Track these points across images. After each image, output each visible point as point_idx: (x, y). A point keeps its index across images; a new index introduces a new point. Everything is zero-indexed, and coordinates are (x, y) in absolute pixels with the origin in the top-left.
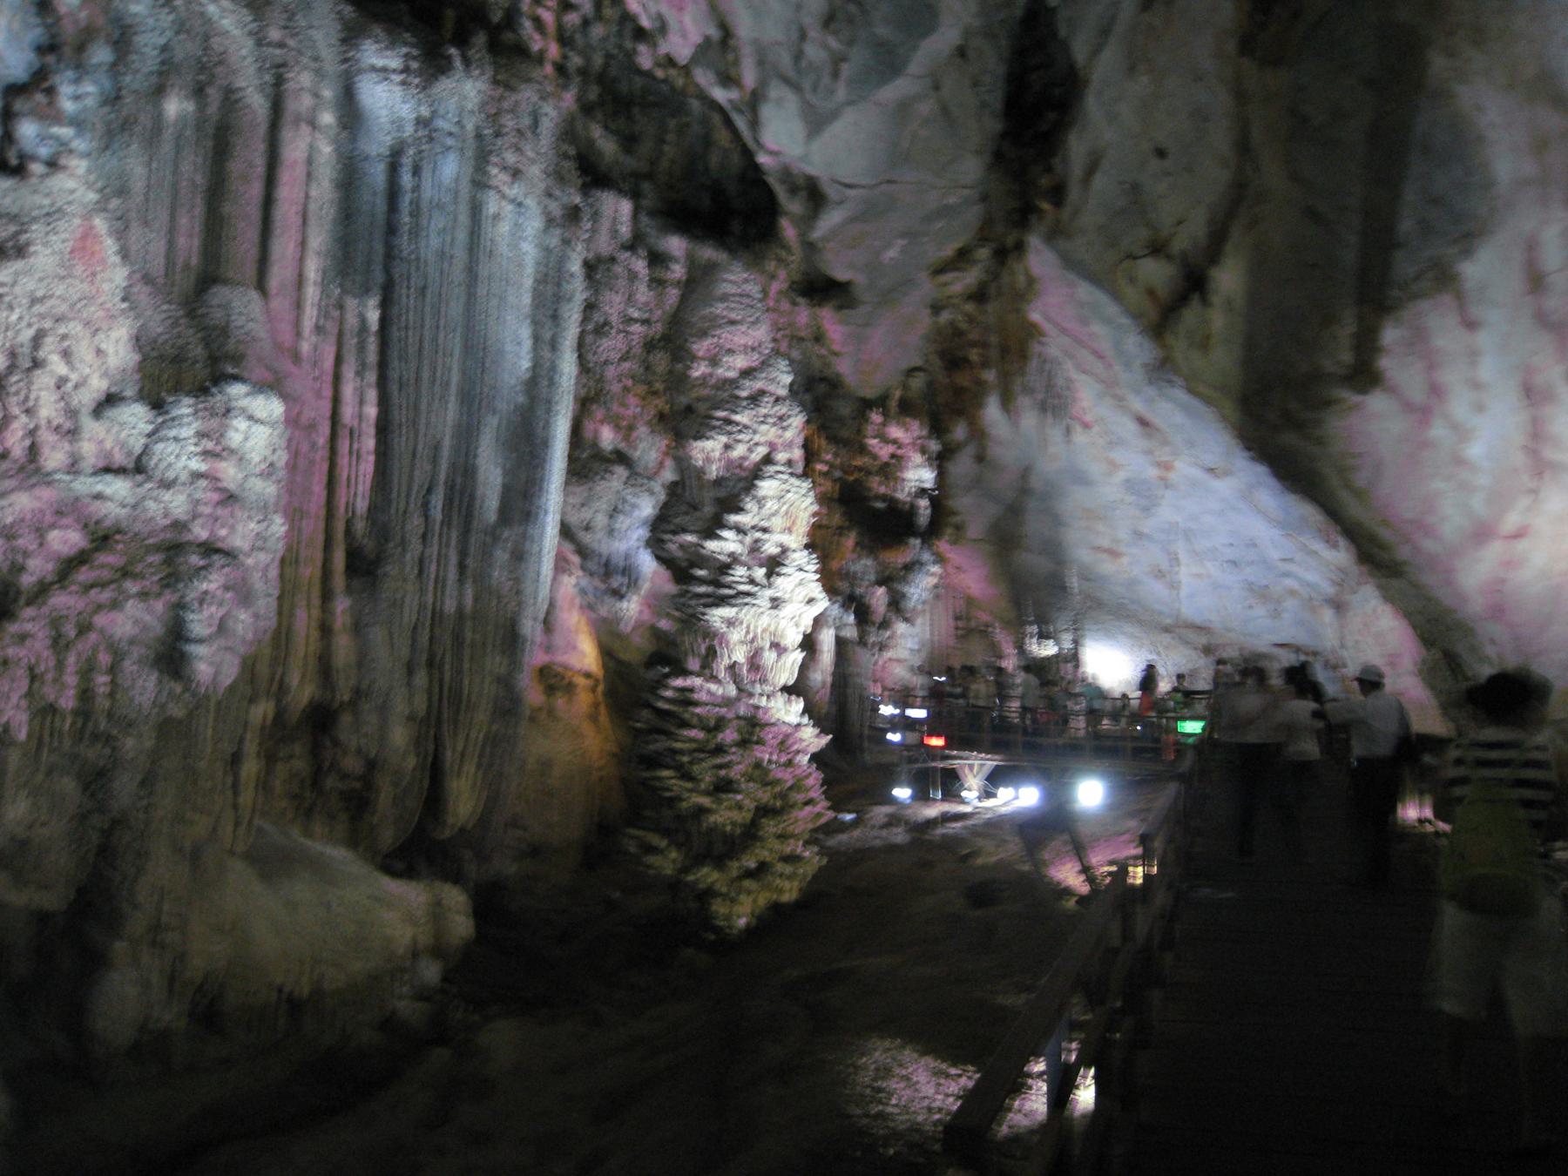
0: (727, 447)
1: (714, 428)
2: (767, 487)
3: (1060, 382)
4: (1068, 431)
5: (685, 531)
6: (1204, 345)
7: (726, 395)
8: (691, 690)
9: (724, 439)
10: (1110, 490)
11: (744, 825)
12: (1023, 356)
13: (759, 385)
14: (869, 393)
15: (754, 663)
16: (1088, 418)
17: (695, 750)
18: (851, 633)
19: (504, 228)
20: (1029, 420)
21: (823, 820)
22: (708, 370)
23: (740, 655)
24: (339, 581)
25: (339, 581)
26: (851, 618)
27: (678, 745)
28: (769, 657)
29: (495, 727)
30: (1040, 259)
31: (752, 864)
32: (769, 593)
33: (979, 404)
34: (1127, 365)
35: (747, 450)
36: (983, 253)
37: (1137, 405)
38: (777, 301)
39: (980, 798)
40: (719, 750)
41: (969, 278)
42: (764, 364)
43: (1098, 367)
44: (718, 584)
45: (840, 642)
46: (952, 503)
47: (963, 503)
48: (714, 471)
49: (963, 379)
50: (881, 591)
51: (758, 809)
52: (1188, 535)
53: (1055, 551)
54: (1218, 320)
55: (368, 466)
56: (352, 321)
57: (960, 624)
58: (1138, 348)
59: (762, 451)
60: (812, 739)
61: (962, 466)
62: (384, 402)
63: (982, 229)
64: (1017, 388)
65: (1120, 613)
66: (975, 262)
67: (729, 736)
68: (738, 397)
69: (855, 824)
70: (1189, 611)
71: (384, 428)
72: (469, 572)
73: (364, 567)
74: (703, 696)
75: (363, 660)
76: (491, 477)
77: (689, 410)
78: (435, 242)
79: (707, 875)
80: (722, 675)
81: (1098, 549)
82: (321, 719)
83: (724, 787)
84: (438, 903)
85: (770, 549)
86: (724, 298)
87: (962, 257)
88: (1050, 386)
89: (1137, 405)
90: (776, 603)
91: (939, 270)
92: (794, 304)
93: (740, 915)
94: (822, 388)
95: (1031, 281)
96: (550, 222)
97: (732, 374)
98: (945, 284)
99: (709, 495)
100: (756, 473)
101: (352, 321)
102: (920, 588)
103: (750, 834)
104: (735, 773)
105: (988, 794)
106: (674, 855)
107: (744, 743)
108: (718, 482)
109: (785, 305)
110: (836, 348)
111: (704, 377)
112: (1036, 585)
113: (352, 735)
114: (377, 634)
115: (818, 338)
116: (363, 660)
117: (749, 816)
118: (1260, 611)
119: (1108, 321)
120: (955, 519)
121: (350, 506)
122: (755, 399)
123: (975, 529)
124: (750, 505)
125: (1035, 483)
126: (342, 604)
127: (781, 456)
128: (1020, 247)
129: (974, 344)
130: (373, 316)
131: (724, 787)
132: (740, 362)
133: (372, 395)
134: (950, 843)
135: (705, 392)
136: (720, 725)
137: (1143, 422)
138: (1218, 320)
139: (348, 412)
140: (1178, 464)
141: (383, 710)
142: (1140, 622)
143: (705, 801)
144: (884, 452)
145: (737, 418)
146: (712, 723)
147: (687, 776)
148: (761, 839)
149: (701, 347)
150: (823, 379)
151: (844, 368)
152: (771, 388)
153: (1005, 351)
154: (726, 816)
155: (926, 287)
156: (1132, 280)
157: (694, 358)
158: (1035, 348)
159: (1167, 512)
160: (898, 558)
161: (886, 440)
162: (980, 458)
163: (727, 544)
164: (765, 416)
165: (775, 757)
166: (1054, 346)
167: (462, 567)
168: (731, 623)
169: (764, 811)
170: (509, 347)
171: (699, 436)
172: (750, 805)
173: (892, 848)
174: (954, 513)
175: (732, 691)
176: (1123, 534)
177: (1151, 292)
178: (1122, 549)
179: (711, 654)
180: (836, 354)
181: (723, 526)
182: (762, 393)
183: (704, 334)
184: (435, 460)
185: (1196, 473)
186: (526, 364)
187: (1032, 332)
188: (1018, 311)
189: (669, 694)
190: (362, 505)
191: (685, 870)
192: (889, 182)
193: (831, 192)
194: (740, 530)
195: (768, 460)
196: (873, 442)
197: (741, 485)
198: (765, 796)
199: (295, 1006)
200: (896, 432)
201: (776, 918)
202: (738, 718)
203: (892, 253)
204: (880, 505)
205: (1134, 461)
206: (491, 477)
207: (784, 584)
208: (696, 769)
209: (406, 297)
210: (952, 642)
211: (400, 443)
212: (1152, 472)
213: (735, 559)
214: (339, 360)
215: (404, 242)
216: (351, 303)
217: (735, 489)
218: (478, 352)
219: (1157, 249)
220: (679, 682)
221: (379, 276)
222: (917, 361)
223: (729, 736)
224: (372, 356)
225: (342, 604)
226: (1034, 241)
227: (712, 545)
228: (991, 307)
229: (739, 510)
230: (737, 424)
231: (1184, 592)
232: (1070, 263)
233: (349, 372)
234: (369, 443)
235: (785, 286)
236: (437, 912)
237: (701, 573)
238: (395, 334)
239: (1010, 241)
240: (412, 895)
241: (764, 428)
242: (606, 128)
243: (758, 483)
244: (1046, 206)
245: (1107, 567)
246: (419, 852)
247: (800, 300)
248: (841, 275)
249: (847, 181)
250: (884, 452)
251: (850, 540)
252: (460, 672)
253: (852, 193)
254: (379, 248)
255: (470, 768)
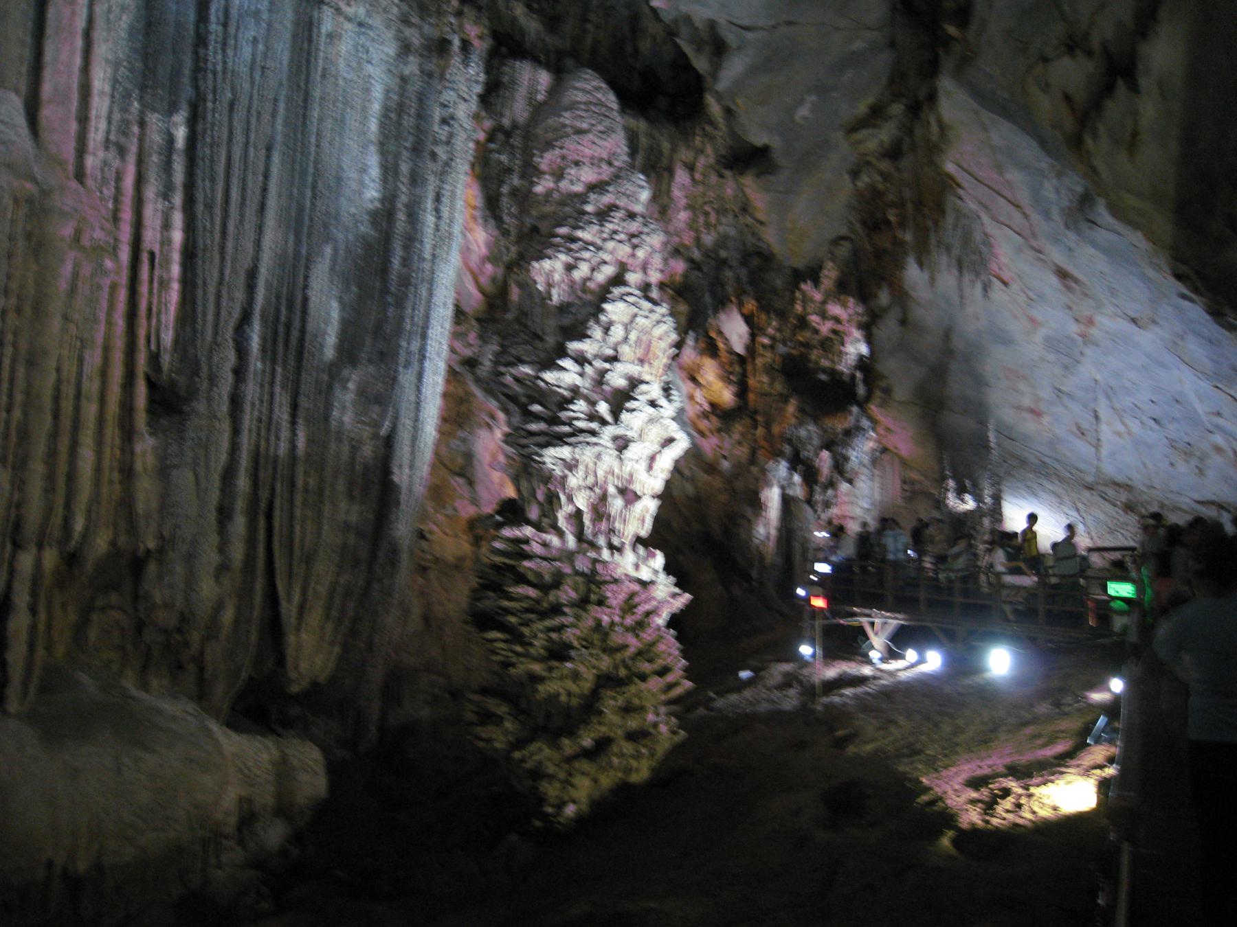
0: (570, 268)
1: (557, 246)
2: (615, 311)
3: (978, 236)
4: (986, 288)
5: (522, 362)
6: (1132, 143)
7: (572, 210)
8: (526, 541)
9: (563, 257)
10: (1032, 348)
11: (581, 696)
12: (940, 209)
13: (607, 199)
14: (799, 263)
15: (600, 510)
16: (1006, 275)
17: (527, 610)
18: (798, 489)
19: (344, 47)
20: (947, 279)
21: (677, 691)
22: (551, 185)
23: (582, 502)
24: (141, 419)
25: (141, 419)
26: (797, 478)
27: (506, 603)
28: (617, 504)
29: (343, 580)
30: (953, 102)
31: (587, 742)
32: (610, 431)
33: (900, 266)
34: (1047, 215)
35: (593, 269)
36: (897, 109)
37: (1057, 256)
38: (704, 175)
39: (883, 660)
40: (556, 610)
41: (884, 135)
42: (617, 177)
43: (1017, 217)
44: (555, 421)
45: (786, 501)
46: (881, 367)
47: (889, 366)
48: (557, 297)
49: (884, 242)
50: (825, 454)
51: (598, 677)
52: (1110, 393)
53: (979, 411)
54: (1149, 109)
55: (174, 294)
56: (155, 138)
57: (906, 487)
58: (1057, 190)
59: (609, 271)
60: (667, 597)
61: (888, 329)
62: (190, 227)
63: (892, 81)
64: (933, 240)
65: (1043, 472)
66: (887, 119)
67: (567, 594)
68: (584, 213)
69: (750, 683)
70: (1109, 469)
71: (190, 254)
72: (301, 413)
73: (168, 403)
74: (536, 548)
75: (165, 505)
76: (328, 313)
77: (535, 230)
78: (247, 51)
79: (541, 753)
80: (562, 523)
81: (1019, 408)
82: (131, 567)
83: (559, 653)
84: (284, 760)
85: (617, 379)
86: (572, 106)
87: (876, 114)
88: (967, 240)
89: (1057, 256)
90: (622, 444)
91: (853, 129)
92: (721, 176)
93: (576, 794)
94: (755, 262)
95: (942, 127)
96: (405, 48)
97: (578, 188)
98: (860, 142)
99: (551, 324)
100: (603, 295)
101: (155, 138)
102: (860, 451)
103: (590, 707)
104: (570, 635)
105: (891, 655)
106: (508, 725)
107: (583, 603)
108: (563, 308)
109: (713, 178)
110: (760, 216)
111: (549, 193)
112: (960, 442)
113: (161, 589)
114: (184, 478)
115: (745, 209)
116: (165, 505)
117: (587, 686)
118: (1182, 468)
119: (1025, 168)
120: (883, 384)
121: (154, 336)
122: (603, 215)
123: (902, 392)
124: (597, 332)
125: (958, 343)
126: (146, 446)
127: (633, 278)
128: (932, 97)
129: (892, 205)
130: (181, 134)
131: (559, 653)
132: (588, 175)
133: (178, 218)
134: (837, 716)
135: (548, 209)
136: (558, 581)
137: (1063, 274)
138: (1149, 109)
139: (151, 237)
140: (1100, 319)
141: (190, 559)
142: (1061, 480)
143: (537, 668)
144: (825, 328)
145: (580, 234)
146: (548, 578)
147: (515, 636)
148: (600, 713)
149: (546, 161)
150: (759, 254)
151: (770, 237)
152: (622, 202)
153: (919, 204)
154: (561, 686)
155: (842, 152)
156: (1046, 87)
157: (540, 173)
158: (951, 201)
159: (1088, 370)
160: (839, 424)
161: (823, 315)
162: (903, 322)
163: (566, 376)
164: (615, 232)
165: (617, 619)
166: (970, 199)
167: (295, 407)
168: (571, 466)
169: (607, 681)
170: (351, 174)
171: (540, 257)
172: (589, 676)
173: (777, 717)
174: (883, 377)
175: (571, 542)
176: (1046, 393)
177: (1067, 98)
178: (1042, 407)
179: (552, 501)
180: (761, 223)
181: (563, 353)
182: (613, 207)
183: (549, 145)
184: (251, 288)
185: (1124, 326)
186: (372, 193)
187: (947, 184)
188: (932, 163)
189: (498, 545)
190: (168, 337)
191: (519, 744)
192: (789, 23)
193: (730, 37)
194: (581, 360)
195: (618, 280)
196: (814, 319)
197: (584, 311)
198: (605, 663)
199: (74, 884)
200: (835, 309)
201: (620, 804)
202: (577, 573)
203: (804, 112)
204: (823, 377)
205: (1055, 318)
206: (328, 313)
207: (634, 420)
208: (526, 631)
209: (216, 112)
210: (900, 502)
211: (209, 271)
212: (1073, 328)
213: (575, 392)
214: (140, 181)
215: (214, 55)
216: (153, 119)
217: (582, 312)
218: (311, 179)
219: (1073, 45)
220: (507, 532)
221: (187, 92)
222: (844, 231)
223: (567, 594)
224: (179, 177)
225: (146, 446)
226: (946, 83)
227: (549, 376)
228: (906, 163)
229: (583, 336)
230: (580, 239)
231: (1104, 451)
232: (983, 98)
233: (151, 192)
234: (176, 270)
235: (712, 160)
236: (283, 771)
237: (536, 408)
238: (203, 151)
239: (923, 93)
240: (250, 754)
241: (610, 245)
242: (529, 7)
243: (606, 306)
244: (951, 30)
245: (1029, 426)
246: (262, 705)
247: (728, 173)
248: (758, 138)
249: (745, 22)
250: (825, 328)
251: (791, 408)
252: (292, 517)
253: (750, 36)
254: (188, 62)
255: (315, 617)
